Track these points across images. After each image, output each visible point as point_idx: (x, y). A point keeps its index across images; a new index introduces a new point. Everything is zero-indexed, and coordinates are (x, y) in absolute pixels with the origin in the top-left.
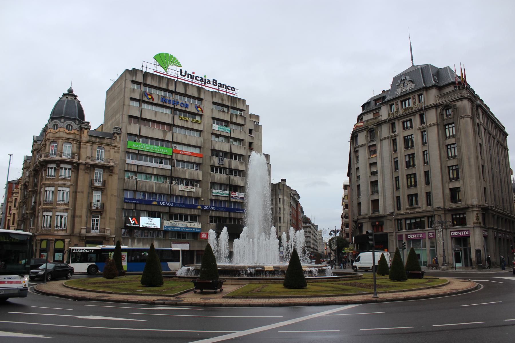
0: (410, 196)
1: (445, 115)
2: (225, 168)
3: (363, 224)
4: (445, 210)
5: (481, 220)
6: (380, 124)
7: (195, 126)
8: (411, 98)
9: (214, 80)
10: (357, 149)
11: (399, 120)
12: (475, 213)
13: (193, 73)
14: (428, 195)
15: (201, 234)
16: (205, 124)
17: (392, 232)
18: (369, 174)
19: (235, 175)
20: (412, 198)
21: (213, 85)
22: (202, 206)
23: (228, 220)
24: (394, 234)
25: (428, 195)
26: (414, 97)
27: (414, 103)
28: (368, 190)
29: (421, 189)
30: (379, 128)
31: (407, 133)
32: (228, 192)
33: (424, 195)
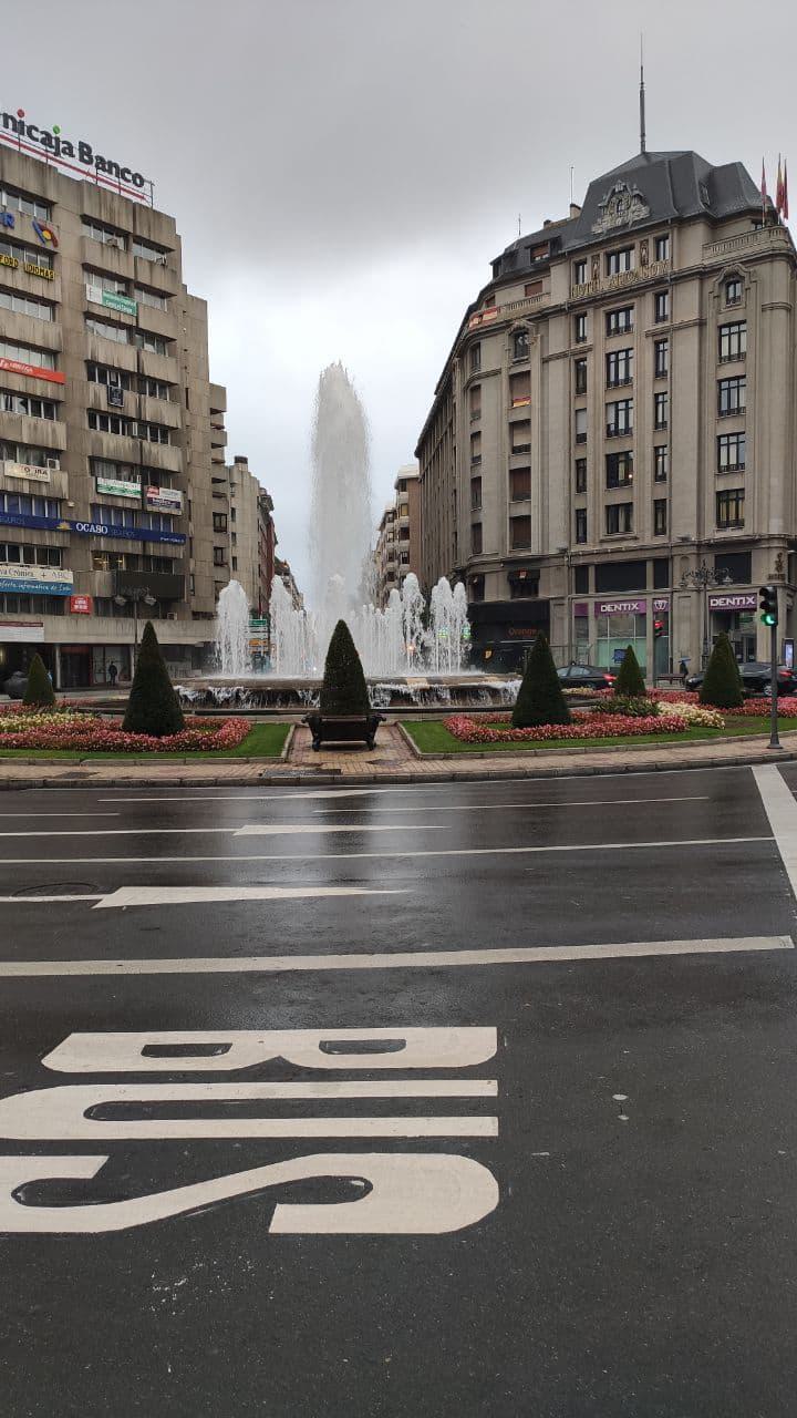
0: (612, 511)
1: (724, 300)
2: (128, 420)
3: (487, 578)
4: (699, 545)
5: (785, 571)
6: (543, 317)
7: (38, 288)
8: (637, 245)
9: (82, 145)
10: (477, 383)
11: (596, 308)
12: (774, 558)
13: (21, 113)
14: (660, 506)
15: (72, 600)
16: (66, 284)
17: (562, 598)
18: (508, 451)
19: (154, 440)
20: (618, 516)
21: (82, 160)
22: (73, 524)
23: (140, 563)
24: (566, 602)
25: (660, 506)
26: (644, 244)
27: (643, 263)
28: (503, 490)
29: (642, 493)
30: (542, 326)
31: (617, 343)
32: (138, 487)
33: (649, 506)
